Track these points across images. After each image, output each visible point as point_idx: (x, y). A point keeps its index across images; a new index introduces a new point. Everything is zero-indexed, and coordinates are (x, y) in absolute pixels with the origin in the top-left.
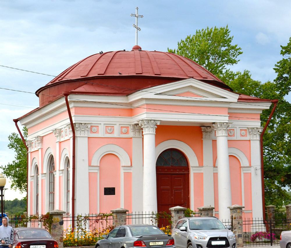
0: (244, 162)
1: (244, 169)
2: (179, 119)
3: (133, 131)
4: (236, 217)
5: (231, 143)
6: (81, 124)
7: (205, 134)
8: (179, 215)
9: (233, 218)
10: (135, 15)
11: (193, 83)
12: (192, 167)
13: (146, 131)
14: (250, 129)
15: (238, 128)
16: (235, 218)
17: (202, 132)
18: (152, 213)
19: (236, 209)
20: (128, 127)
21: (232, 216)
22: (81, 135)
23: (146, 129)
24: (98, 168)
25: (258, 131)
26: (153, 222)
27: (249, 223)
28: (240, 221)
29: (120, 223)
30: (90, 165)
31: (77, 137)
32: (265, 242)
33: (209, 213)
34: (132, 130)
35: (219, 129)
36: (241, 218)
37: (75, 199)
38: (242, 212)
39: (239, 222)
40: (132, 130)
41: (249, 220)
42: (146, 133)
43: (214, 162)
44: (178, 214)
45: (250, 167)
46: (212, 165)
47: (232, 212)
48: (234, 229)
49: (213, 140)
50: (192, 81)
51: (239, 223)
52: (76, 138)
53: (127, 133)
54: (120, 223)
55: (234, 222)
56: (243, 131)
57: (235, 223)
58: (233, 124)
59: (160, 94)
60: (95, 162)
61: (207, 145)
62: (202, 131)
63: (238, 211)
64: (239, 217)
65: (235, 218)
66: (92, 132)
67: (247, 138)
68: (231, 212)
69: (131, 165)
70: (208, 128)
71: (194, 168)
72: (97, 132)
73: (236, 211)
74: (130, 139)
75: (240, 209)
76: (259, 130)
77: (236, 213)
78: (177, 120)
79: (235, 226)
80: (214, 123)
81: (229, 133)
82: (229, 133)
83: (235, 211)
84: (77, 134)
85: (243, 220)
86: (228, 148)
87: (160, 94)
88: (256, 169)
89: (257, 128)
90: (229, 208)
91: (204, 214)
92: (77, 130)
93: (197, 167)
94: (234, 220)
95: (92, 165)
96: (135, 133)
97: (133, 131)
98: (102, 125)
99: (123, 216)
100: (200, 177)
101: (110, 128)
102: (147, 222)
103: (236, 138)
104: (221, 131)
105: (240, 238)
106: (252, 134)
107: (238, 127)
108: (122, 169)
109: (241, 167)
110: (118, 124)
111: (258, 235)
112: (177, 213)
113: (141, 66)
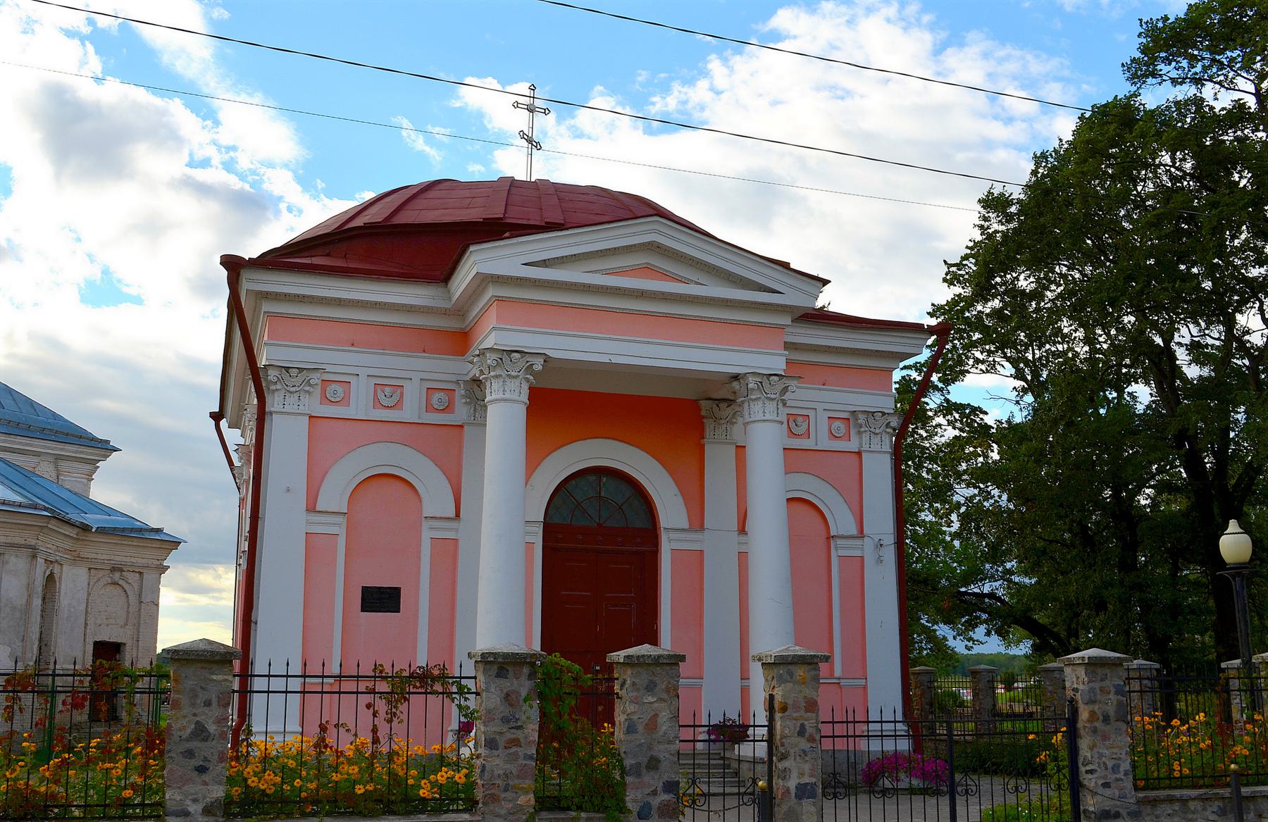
0: (841, 521)
1: (839, 542)
2: (610, 357)
3: (466, 403)
4: (790, 702)
5: (794, 459)
6: (287, 369)
7: (712, 427)
8: (507, 684)
9: (777, 706)
10: (519, 105)
11: (660, 233)
12: (665, 529)
13: (493, 391)
14: (860, 416)
15: (820, 411)
16: (784, 709)
17: (703, 417)
18: (374, 670)
19: (790, 667)
20: (454, 390)
21: (772, 697)
22: (287, 409)
23: (496, 385)
24: (341, 520)
25: (888, 425)
26: (375, 715)
27: (851, 725)
28: (806, 723)
29: (195, 715)
30: (311, 508)
31: (271, 413)
32: (912, 791)
33: (657, 679)
34: (464, 401)
35: (753, 397)
36: (812, 706)
37: (253, 619)
38: (816, 679)
39: (802, 726)
40: (464, 401)
41: (850, 719)
42: (494, 396)
43: (741, 518)
44: (500, 681)
45: (861, 534)
46: (734, 526)
47: (770, 678)
48: (780, 760)
49: (737, 446)
50: (656, 226)
51: (802, 732)
52: (267, 418)
53: (448, 409)
54: (195, 715)
55: (778, 725)
56: (837, 423)
57: (782, 731)
58: (785, 330)
59: (544, 263)
60: (334, 495)
61: (718, 459)
62: (703, 413)
63: (800, 672)
64: (803, 704)
65: (784, 709)
66: (325, 399)
67: (853, 445)
68: (767, 680)
69: (458, 515)
70: (723, 405)
71: (673, 535)
72: (345, 401)
73: (791, 674)
74: (458, 428)
75: (810, 664)
76: (890, 419)
77: (790, 685)
78: (605, 359)
79: (783, 745)
80: (736, 377)
81: (792, 425)
82: (792, 425)
83: (786, 677)
84: (273, 403)
85: (825, 715)
86: (786, 473)
87: (544, 263)
88: (881, 545)
89: (884, 414)
90: (759, 660)
91: (634, 684)
92: (274, 391)
93: (683, 530)
94: (778, 715)
95: (319, 508)
96: (475, 410)
97: (466, 403)
98: (363, 378)
99: (214, 677)
100: (694, 563)
101: (388, 390)
102: (502, 708)
103: (814, 443)
104: (760, 403)
105: (805, 802)
106: (866, 431)
107: (820, 407)
108: (425, 525)
109: (829, 538)
110: (416, 377)
111: (891, 763)
112: (498, 676)
113: (506, 201)
